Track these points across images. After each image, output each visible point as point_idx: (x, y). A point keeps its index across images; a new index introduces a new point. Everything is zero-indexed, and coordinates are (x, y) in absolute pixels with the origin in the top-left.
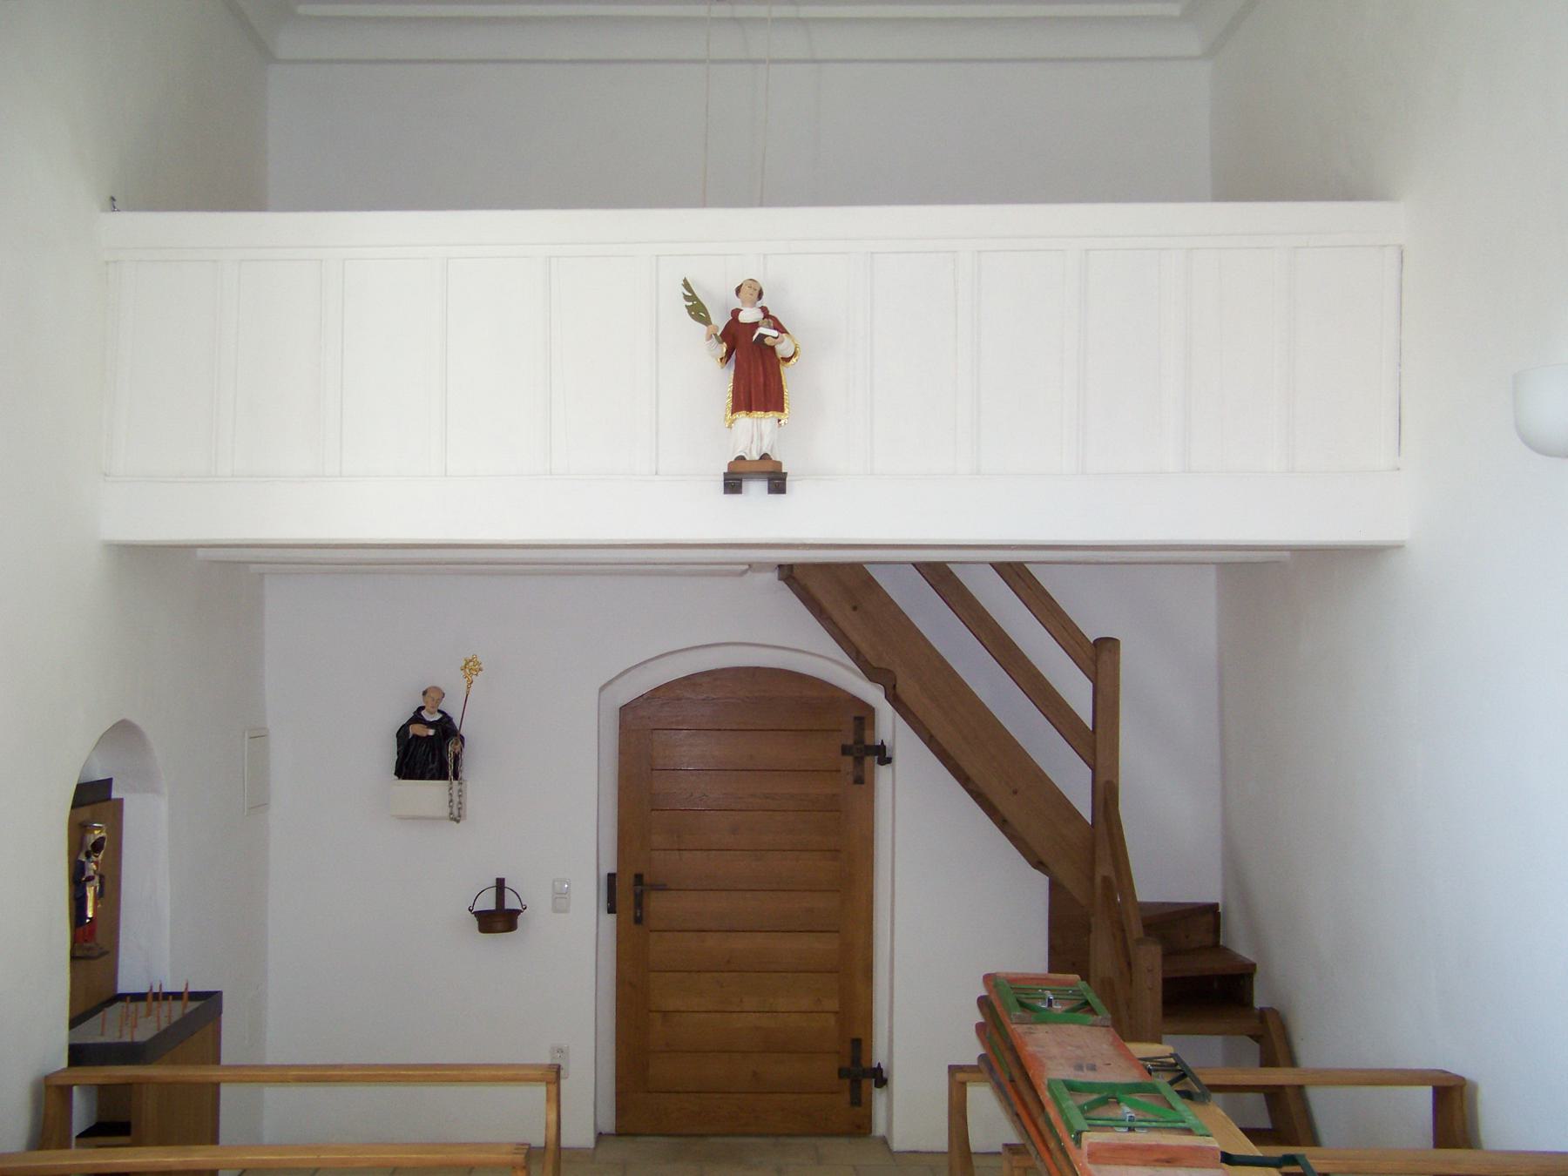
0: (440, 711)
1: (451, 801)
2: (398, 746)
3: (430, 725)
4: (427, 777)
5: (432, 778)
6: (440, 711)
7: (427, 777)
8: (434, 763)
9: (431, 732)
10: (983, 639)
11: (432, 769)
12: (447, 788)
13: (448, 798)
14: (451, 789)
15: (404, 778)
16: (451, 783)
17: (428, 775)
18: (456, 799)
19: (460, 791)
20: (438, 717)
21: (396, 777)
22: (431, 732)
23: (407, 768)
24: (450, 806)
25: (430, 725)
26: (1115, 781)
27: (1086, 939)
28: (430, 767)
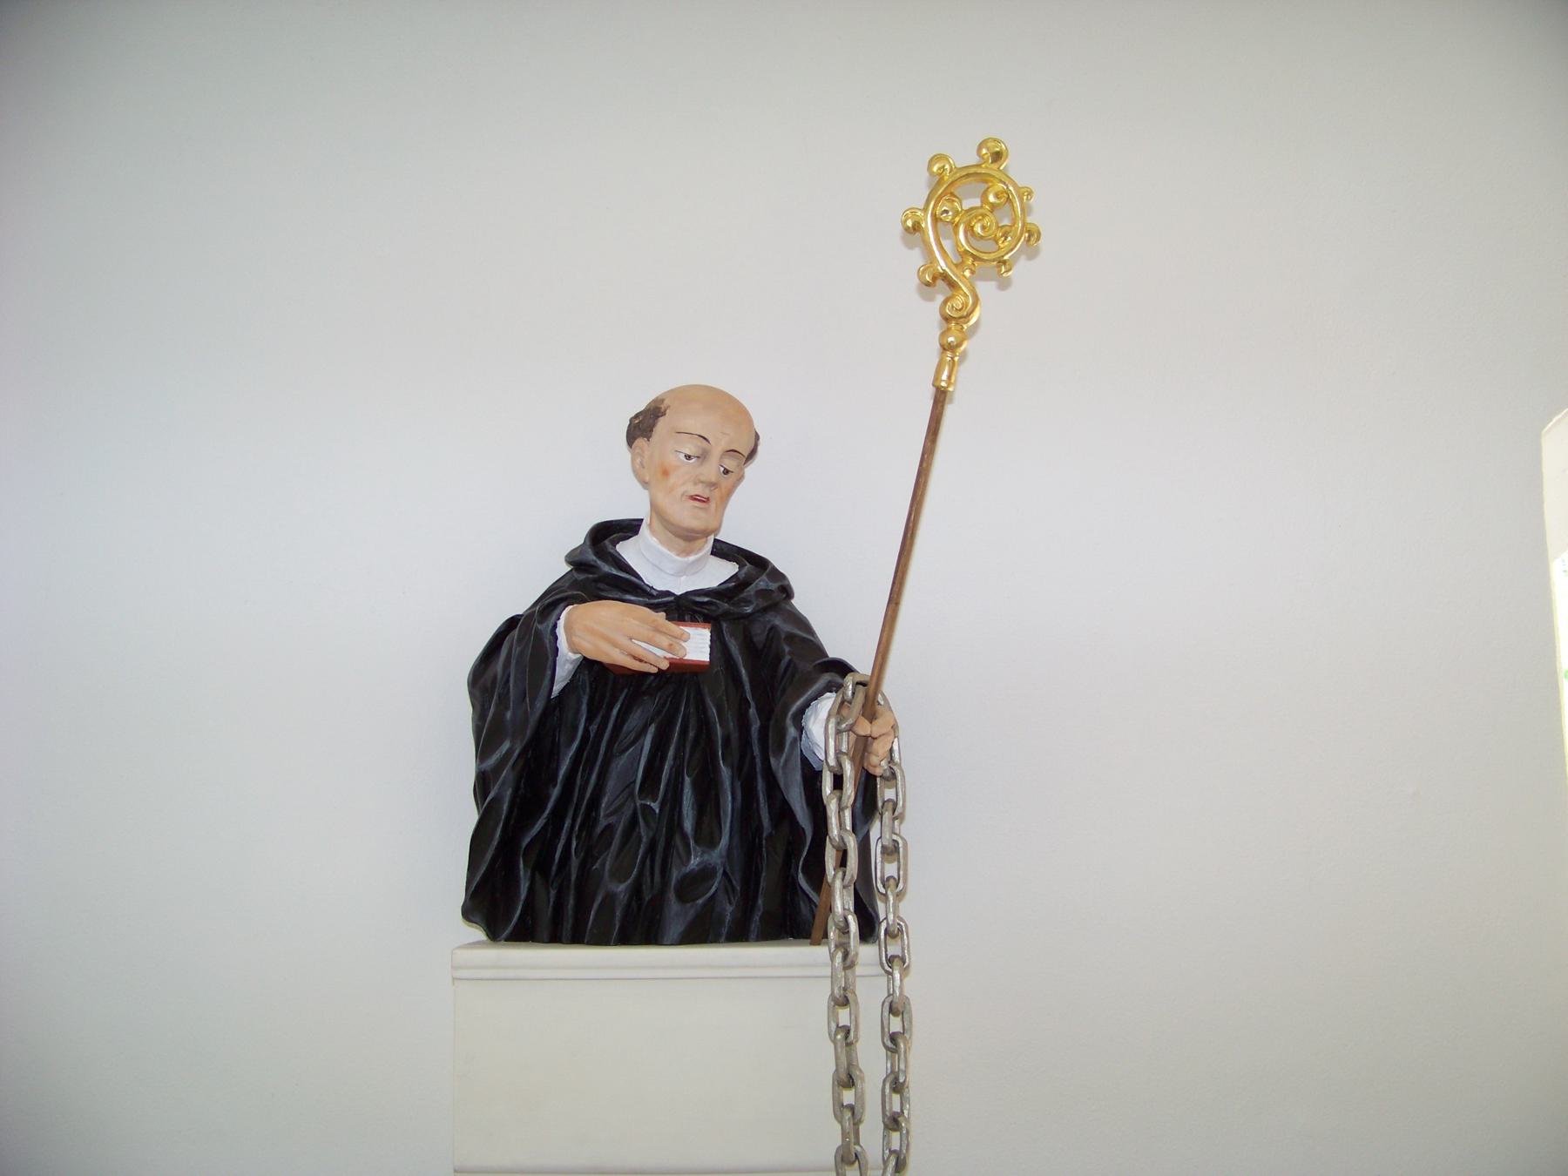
0: (723, 551)
1: (847, 1079)
2: (486, 739)
3: (682, 608)
4: (676, 928)
5: (699, 933)
6: (723, 551)
7: (676, 928)
8: (712, 843)
9: (697, 644)
10: (882, 646)
11: (705, 873)
12: (822, 994)
13: (825, 1061)
14: (843, 1000)
15: (525, 934)
16: (849, 963)
17: (676, 914)
18: (872, 1062)
19: (895, 1008)
20: (719, 573)
21: (478, 934)
22: (697, 644)
23: (541, 867)
24: (839, 1107)
25: (682, 608)
26: (588, 543)
27: (651, 421)
28: (694, 862)
